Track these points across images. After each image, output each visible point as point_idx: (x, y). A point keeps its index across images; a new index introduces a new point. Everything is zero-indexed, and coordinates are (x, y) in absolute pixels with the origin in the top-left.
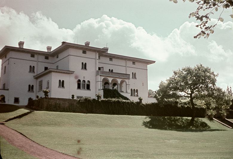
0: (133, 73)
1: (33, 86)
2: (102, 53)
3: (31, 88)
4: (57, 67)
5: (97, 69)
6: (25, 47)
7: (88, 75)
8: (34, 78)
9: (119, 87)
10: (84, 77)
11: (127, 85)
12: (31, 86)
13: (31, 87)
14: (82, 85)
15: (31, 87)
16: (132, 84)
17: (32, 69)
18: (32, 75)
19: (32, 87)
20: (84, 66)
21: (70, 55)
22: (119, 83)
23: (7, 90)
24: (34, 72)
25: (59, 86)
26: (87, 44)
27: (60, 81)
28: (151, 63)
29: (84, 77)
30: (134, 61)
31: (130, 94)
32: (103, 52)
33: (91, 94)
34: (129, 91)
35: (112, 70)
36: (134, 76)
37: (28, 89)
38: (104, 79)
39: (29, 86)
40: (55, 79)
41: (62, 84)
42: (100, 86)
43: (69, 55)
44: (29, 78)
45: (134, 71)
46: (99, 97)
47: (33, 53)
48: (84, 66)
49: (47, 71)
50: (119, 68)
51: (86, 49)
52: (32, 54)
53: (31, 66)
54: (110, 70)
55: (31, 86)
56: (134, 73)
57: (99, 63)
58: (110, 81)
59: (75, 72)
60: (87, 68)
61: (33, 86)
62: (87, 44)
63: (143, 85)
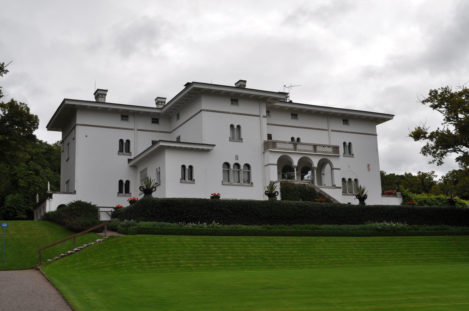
0: (344, 143)
1: (128, 182)
2: (274, 104)
3: (124, 187)
4: (179, 138)
5: (266, 139)
6: (109, 99)
7: (249, 151)
8: (131, 166)
9: (316, 177)
10: (237, 157)
11: (332, 169)
12: (124, 182)
13: (124, 186)
14: (237, 172)
15: (124, 186)
16: (343, 168)
17: (124, 147)
18: (124, 158)
19: (126, 184)
20: (236, 132)
21: (204, 110)
22: (315, 165)
23: (72, 193)
24: (128, 150)
25: (181, 179)
26: (241, 84)
27: (183, 167)
28: (384, 120)
29: (237, 157)
30: (346, 117)
31: (341, 190)
32: (276, 99)
33: (255, 193)
34: (339, 183)
35: (298, 139)
36: (348, 147)
37: (117, 190)
38: (280, 160)
39: (121, 182)
40: (172, 164)
41: (187, 174)
42: (273, 175)
43: (201, 111)
44: (120, 167)
45: (348, 138)
46: (271, 194)
47: (126, 113)
48: (236, 132)
49: (156, 151)
50: (313, 135)
51: (238, 95)
52: (154, 117)
53: (121, 141)
54: (293, 139)
55: (124, 182)
56: (348, 144)
57: (268, 124)
58: (295, 163)
59: (394, 117)
60: (195, 177)
61: (128, 182)
62: (241, 84)
63: (369, 170)
